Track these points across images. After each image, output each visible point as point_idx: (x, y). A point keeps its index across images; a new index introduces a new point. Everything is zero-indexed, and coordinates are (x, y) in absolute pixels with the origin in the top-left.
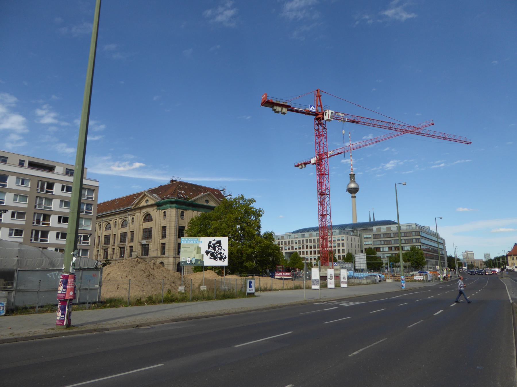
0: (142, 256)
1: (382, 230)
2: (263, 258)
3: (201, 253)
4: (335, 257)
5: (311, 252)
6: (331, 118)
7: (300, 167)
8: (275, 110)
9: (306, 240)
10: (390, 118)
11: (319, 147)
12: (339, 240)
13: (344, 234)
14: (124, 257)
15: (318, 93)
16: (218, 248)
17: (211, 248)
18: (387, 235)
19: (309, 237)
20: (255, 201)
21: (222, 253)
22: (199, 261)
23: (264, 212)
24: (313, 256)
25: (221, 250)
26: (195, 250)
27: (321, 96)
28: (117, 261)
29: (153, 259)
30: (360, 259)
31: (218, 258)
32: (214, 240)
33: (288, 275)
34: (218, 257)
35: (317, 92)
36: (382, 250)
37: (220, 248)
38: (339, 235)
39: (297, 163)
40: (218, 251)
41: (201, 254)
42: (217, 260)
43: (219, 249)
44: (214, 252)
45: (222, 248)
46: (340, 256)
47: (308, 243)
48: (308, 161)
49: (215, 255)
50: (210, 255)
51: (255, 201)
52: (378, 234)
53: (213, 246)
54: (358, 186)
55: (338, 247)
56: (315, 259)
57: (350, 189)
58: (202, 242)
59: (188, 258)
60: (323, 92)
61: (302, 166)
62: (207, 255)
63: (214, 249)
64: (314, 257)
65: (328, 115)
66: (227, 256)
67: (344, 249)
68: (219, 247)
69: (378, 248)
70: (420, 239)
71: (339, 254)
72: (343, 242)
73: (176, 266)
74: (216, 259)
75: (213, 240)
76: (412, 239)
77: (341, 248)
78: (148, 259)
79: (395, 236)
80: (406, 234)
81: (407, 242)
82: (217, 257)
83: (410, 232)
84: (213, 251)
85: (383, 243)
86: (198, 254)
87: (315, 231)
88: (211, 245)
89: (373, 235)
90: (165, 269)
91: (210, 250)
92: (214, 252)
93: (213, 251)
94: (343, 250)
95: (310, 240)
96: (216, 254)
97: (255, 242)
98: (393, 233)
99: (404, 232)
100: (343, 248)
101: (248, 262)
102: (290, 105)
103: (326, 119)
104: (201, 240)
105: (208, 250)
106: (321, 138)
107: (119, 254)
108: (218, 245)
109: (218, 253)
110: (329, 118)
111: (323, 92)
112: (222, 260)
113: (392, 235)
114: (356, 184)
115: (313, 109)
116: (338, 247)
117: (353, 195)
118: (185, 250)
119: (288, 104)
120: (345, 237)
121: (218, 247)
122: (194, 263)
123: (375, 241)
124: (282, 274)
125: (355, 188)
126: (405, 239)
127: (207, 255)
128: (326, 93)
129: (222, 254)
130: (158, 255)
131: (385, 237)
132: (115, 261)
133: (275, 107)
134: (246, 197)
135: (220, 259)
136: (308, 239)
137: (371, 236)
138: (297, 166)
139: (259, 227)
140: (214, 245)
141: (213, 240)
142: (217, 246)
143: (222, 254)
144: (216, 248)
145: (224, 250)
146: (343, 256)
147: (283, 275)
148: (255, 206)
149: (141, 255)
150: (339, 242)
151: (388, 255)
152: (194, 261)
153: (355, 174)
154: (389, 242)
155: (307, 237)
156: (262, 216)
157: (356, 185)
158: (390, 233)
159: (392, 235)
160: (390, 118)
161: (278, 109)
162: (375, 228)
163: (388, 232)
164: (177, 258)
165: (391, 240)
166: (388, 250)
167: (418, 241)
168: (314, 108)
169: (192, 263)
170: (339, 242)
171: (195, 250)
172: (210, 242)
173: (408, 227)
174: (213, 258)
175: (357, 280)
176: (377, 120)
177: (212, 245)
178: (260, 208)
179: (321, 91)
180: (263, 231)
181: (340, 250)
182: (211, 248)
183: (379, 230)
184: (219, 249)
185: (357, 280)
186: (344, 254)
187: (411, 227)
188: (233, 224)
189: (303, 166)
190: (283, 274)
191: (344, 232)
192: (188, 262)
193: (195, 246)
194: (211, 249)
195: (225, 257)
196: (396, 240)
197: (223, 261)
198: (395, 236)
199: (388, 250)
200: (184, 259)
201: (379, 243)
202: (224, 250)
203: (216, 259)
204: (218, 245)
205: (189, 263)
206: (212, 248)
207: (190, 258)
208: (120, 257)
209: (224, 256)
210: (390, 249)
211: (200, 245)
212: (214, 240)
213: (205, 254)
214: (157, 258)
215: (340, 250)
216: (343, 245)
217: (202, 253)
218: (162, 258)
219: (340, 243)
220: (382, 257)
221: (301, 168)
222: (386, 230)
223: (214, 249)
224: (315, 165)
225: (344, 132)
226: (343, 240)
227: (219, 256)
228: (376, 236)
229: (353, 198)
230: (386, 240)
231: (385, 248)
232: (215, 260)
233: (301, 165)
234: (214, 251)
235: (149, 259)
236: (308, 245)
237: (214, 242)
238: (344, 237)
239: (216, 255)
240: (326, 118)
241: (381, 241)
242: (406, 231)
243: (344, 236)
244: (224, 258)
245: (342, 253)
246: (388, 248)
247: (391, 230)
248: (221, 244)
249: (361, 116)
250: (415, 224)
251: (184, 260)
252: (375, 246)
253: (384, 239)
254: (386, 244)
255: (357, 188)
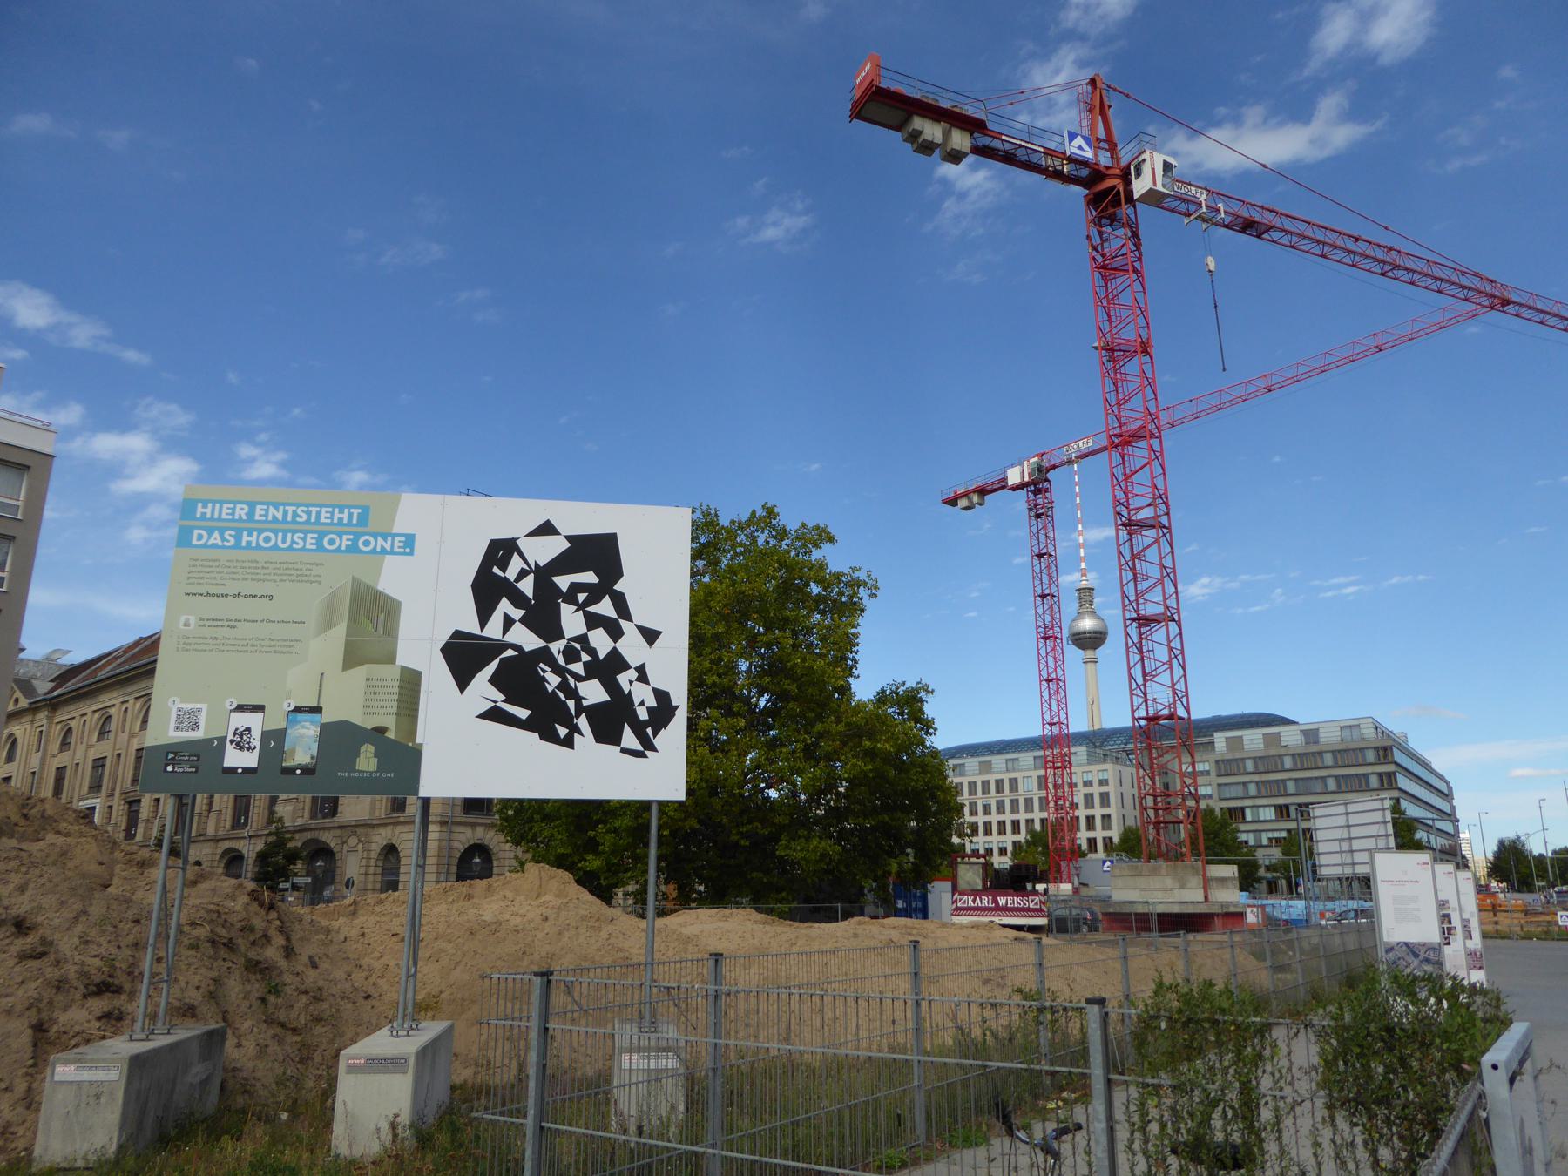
0: (311, 818)
1: (1285, 740)
2: (880, 818)
3: (391, 659)
4: (1078, 842)
5: (1002, 824)
6: (1164, 186)
7: (963, 503)
8: (914, 136)
9: (969, 783)
10: (1386, 228)
11: (1110, 320)
12: (1088, 784)
13: (1105, 761)
14: (246, 823)
15: (1098, 90)
16: (581, 607)
17: (505, 606)
18: (1267, 763)
19: (980, 774)
20: (831, 539)
21: (625, 666)
22: (368, 750)
23: (877, 588)
24: (995, 840)
25: (615, 633)
26: (328, 623)
27: (1110, 107)
28: (220, 844)
29: (354, 834)
30: (1348, 826)
31: (582, 722)
32: (547, 529)
33: (1029, 909)
34: (580, 709)
35: (1089, 87)
36: (1252, 815)
37: (605, 608)
38: (1089, 764)
39: (953, 489)
40: (583, 639)
41: (391, 673)
42: (568, 743)
43: (590, 628)
44: (544, 655)
45: (620, 602)
46: (1095, 839)
47: (976, 794)
48: (993, 478)
49: (553, 680)
50: (494, 681)
51: (831, 539)
52: (1236, 760)
53: (527, 586)
54: (1106, 627)
55: (1087, 807)
56: (1003, 851)
57: (1079, 634)
58: (409, 541)
59: (241, 708)
60: (1115, 90)
61: (970, 500)
62: (462, 687)
63: (543, 618)
64: (1000, 845)
65: (1153, 170)
66: (680, 697)
67: (1109, 816)
68: (595, 597)
69: (1235, 809)
70: (1394, 773)
71: (1091, 834)
72: (1104, 789)
73: (455, 862)
74: (562, 731)
75: (532, 534)
76: (1366, 776)
77: (1098, 812)
78: (333, 832)
79: (1299, 766)
80: (1339, 757)
81: (1344, 788)
82: (571, 704)
83: (1353, 750)
84: (529, 641)
85: (1252, 790)
86: (361, 672)
87: (999, 752)
88: (511, 573)
89: (1217, 762)
90: (93, 848)
91: (494, 629)
92: (544, 655)
93: (529, 641)
94: (1106, 818)
95: (986, 784)
96: (558, 670)
97: (841, 727)
98: (1293, 755)
99: (1333, 752)
100: (1106, 811)
101: (803, 840)
102: (982, 116)
103: (1143, 191)
104: (397, 528)
105: (472, 626)
106: (1120, 281)
107: (230, 812)
108: (590, 577)
109: (578, 668)
110: (1155, 184)
111: (1115, 90)
112: (629, 739)
113: (1288, 763)
114: (1099, 618)
115: (1080, 148)
116: (1087, 807)
117: (1090, 654)
118: (215, 622)
119: (970, 110)
120: (1110, 772)
121: (588, 602)
122: (307, 771)
123: (1226, 784)
124: (995, 901)
125: (1095, 632)
126: (1336, 777)
127: (462, 687)
128: (1127, 96)
129: (624, 679)
130: (377, 814)
131: (1261, 769)
132: (212, 844)
133: (917, 123)
134: (789, 519)
135: (607, 732)
136: (979, 779)
137: (1207, 769)
138: (952, 502)
139: (850, 671)
140: (544, 575)
141: (532, 534)
142: (576, 588)
143: (624, 679)
144: (567, 610)
145: (650, 636)
146: (1104, 839)
147: (998, 909)
148: (835, 558)
149: (307, 814)
150: (1088, 790)
151: (1276, 835)
152: (303, 745)
153: (1093, 589)
154: (1278, 788)
155: (974, 775)
156: (863, 611)
157: (1100, 622)
158: (1280, 756)
159: (1288, 763)
160: (1386, 228)
161: (932, 131)
162: (1220, 739)
163: (1273, 752)
164: (457, 829)
165: (1283, 781)
166: (1274, 818)
167: (1390, 783)
168: (1085, 146)
169: (287, 764)
170: (1088, 790)
171: (328, 623)
172: (501, 551)
173: (1346, 733)
174: (523, 713)
175: (1344, 944)
176: (1339, 229)
177: (522, 574)
178: (854, 569)
179: (1109, 87)
180: (864, 688)
181: (1093, 817)
182: (505, 606)
183: (1235, 744)
184: (590, 628)
185: (1344, 944)
186: (1107, 834)
187: (1355, 733)
188: (721, 628)
189: (975, 498)
190: (1002, 902)
191: (1104, 755)
192: (235, 758)
193: (338, 577)
194: (508, 622)
195: (663, 711)
196: (1302, 779)
197: (638, 746)
198: (1299, 766)
199: (1274, 818)
200: (188, 719)
201: (1239, 791)
202: (650, 636)
203: (562, 731)
204: (590, 577)
205: (250, 759)
206: (517, 614)
207: (259, 708)
208: (233, 827)
209: (643, 696)
210: (1283, 811)
211: (392, 579)
212: (547, 529)
213: (437, 676)
214: (373, 826)
215: (1093, 817)
216: (1105, 799)
217: (402, 660)
218: (390, 827)
219: (1092, 795)
220: (1251, 843)
221: (967, 508)
222: (1262, 745)
223: (543, 618)
224: (1022, 493)
225: (1211, 263)
226: (1103, 782)
227: (593, 692)
228: (1227, 767)
229: (1089, 664)
230: (1263, 782)
231: (1261, 810)
232: (549, 736)
233: (966, 495)
234: (540, 643)
235: (338, 832)
236: (976, 803)
237: (543, 551)
238: (1109, 770)
239: (563, 686)
240: (1140, 187)
241: (1245, 784)
242: (1340, 748)
243: (1109, 766)
244: (643, 714)
245: (1103, 829)
246: (1273, 809)
247: (1283, 744)
248: (618, 574)
249: (1275, 208)
250: (1371, 720)
251: (195, 726)
252: (1225, 804)
253: (1256, 778)
254: (1264, 794)
255: (1101, 633)
